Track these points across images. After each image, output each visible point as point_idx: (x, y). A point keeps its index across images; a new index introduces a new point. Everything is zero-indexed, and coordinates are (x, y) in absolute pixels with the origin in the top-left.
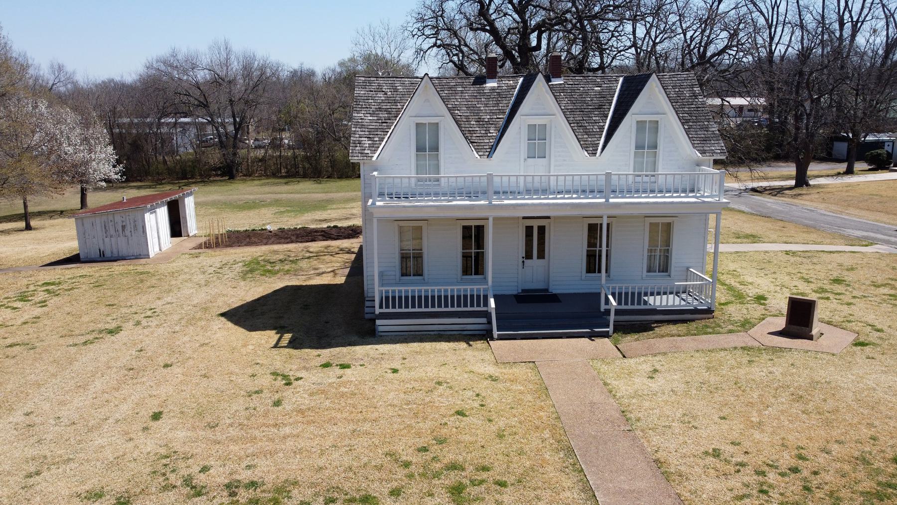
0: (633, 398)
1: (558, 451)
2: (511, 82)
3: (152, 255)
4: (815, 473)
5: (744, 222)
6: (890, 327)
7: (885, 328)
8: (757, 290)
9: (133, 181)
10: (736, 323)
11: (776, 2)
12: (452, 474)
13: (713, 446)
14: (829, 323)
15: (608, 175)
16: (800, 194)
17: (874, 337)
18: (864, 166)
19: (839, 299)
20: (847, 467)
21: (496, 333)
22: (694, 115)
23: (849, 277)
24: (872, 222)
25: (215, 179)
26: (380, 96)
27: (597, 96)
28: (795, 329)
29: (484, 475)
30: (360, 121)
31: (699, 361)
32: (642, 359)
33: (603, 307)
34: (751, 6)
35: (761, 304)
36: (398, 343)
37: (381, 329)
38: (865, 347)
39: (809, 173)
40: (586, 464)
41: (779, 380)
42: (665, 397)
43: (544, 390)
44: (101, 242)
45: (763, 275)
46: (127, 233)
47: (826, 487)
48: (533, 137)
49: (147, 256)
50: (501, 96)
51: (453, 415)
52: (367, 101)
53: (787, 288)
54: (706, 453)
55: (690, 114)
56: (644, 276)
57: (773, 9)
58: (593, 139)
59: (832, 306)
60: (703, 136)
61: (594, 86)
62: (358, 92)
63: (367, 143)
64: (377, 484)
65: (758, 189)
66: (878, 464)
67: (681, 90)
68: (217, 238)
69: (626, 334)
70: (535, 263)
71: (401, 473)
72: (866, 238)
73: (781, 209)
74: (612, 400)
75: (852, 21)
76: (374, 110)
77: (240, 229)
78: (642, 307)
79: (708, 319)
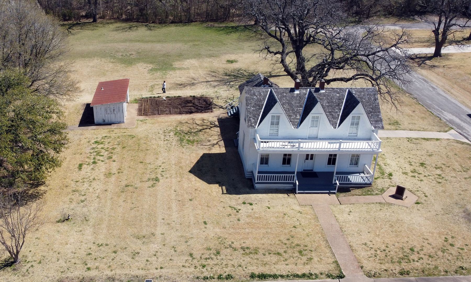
0: (344, 222)
1: (324, 241)
2: (305, 91)
4: (389, 252)
8: (390, 170)
10: (379, 190)
12: (298, 247)
13: (365, 242)
20: (398, 250)
21: (297, 191)
23: (428, 161)
28: (398, 195)
29: (306, 248)
31: (364, 208)
32: (347, 205)
33: (334, 182)
37: (257, 187)
40: (332, 246)
42: (353, 223)
43: (316, 218)
44: (104, 116)
45: (394, 159)
46: (116, 113)
47: (391, 256)
51: (293, 228)
53: (402, 169)
54: (363, 244)
55: (372, 109)
56: (348, 166)
64: (279, 249)
66: (406, 250)
71: (285, 246)
74: (337, 223)
78: (349, 182)
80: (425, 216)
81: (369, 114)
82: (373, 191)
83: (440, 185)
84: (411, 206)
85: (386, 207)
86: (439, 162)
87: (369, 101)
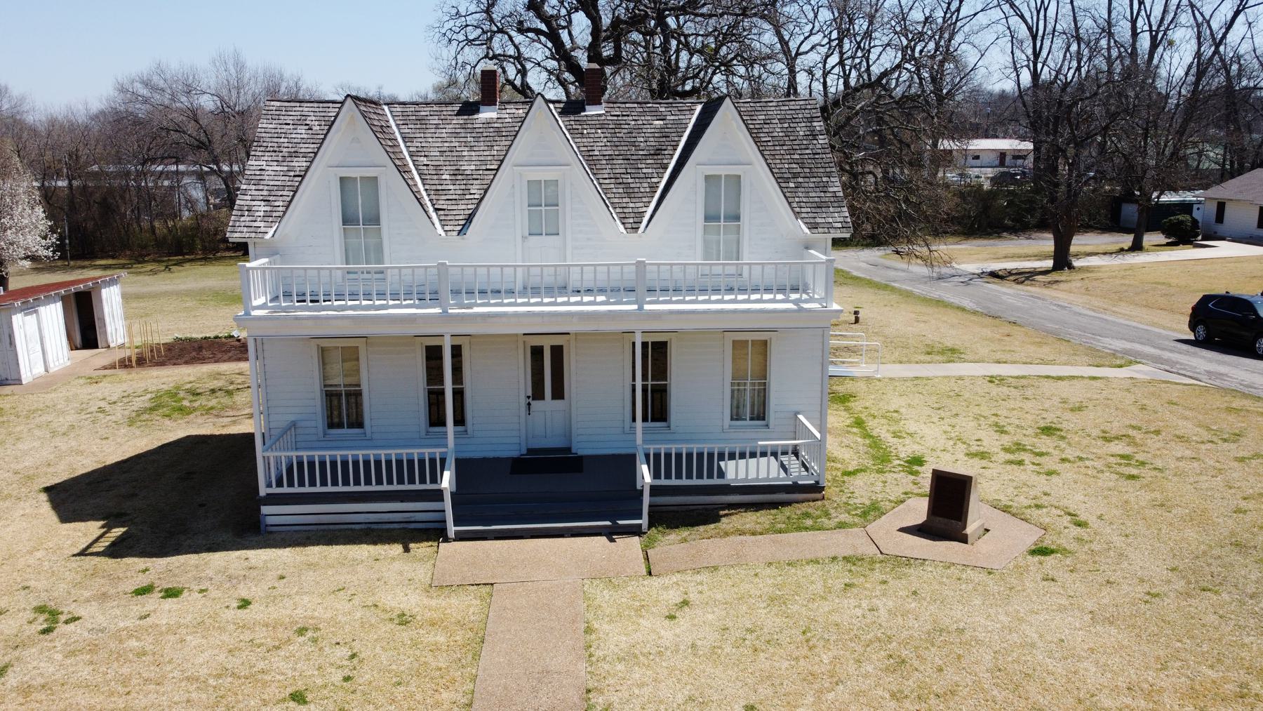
3: (26, 376)
5: (952, 326)
6: (1100, 517)
7: (1092, 520)
8: (916, 447)
9: (102, 258)
10: (856, 509)
11: (1042, 2)
14: (1006, 509)
15: (641, 265)
16: (1057, 282)
17: (1067, 536)
18: (1159, 238)
19: (1038, 464)
21: (452, 529)
22: (807, 165)
23: (1070, 422)
24: (1146, 327)
25: (224, 254)
26: (299, 131)
27: (656, 135)
28: (940, 521)
30: (258, 173)
31: (767, 581)
34: (1006, 7)
35: (912, 473)
36: (289, 546)
37: (270, 520)
38: (1047, 558)
39: (1073, 249)
41: (880, 625)
45: (935, 419)
48: (536, 201)
49: (18, 381)
50: (500, 134)
52: (276, 140)
53: (964, 443)
56: (726, 426)
57: (1038, 12)
58: (638, 205)
59: (1023, 477)
60: (817, 199)
61: (655, 118)
62: (264, 126)
63: (261, 208)
65: (1000, 273)
67: (792, 125)
68: (152, 351)
69: (672, 528)
70: (548, 404)
72: (1126, 352)
73: (1020, 304)
75: (1151, 30)
76: (286, 154)
77: (194, 336)
78: (716, 481)
79: (814, 501)
80: (1089, 605)
81: (787, 180)
82: (827, 514)
83: (1137, 484)
84: (1011, 566)
85: (878, 575)
86: (1116, 424)
87: (787, 139)
